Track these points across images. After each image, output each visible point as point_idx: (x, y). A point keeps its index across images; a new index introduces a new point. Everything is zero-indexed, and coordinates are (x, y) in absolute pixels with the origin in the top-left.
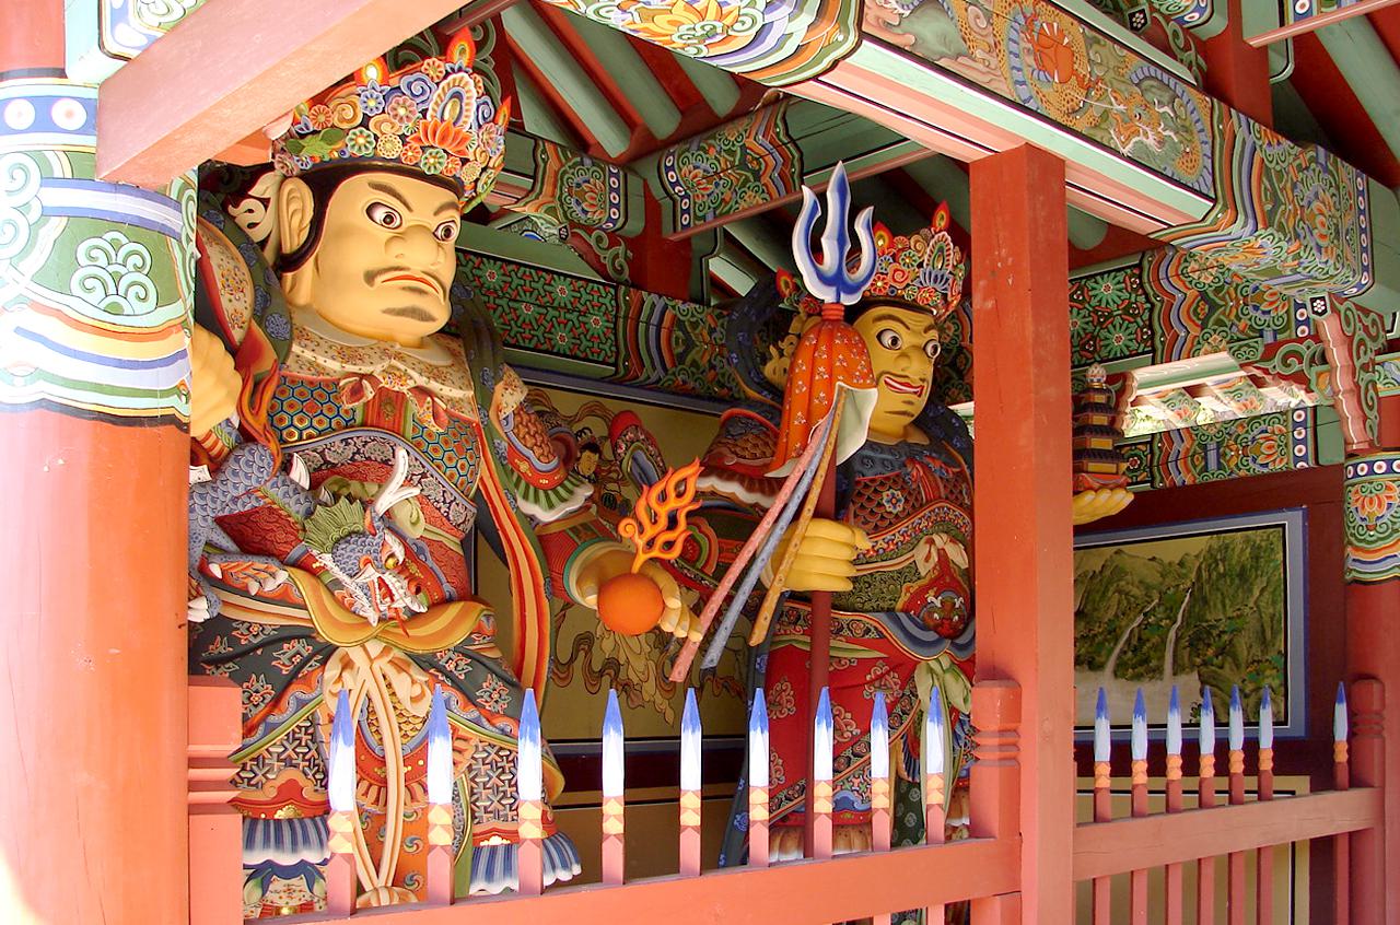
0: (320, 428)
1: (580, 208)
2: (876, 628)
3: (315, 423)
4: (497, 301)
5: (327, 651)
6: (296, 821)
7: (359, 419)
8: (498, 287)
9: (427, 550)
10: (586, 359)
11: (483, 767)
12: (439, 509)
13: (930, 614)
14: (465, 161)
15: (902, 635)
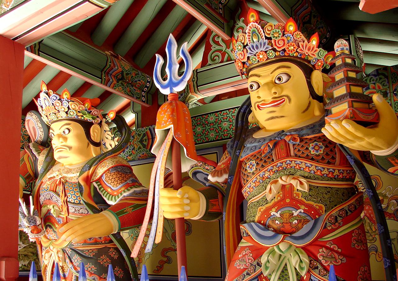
2: (245, 231)
10: (222, 139)
13: (273, 221)
15: (254, 234)
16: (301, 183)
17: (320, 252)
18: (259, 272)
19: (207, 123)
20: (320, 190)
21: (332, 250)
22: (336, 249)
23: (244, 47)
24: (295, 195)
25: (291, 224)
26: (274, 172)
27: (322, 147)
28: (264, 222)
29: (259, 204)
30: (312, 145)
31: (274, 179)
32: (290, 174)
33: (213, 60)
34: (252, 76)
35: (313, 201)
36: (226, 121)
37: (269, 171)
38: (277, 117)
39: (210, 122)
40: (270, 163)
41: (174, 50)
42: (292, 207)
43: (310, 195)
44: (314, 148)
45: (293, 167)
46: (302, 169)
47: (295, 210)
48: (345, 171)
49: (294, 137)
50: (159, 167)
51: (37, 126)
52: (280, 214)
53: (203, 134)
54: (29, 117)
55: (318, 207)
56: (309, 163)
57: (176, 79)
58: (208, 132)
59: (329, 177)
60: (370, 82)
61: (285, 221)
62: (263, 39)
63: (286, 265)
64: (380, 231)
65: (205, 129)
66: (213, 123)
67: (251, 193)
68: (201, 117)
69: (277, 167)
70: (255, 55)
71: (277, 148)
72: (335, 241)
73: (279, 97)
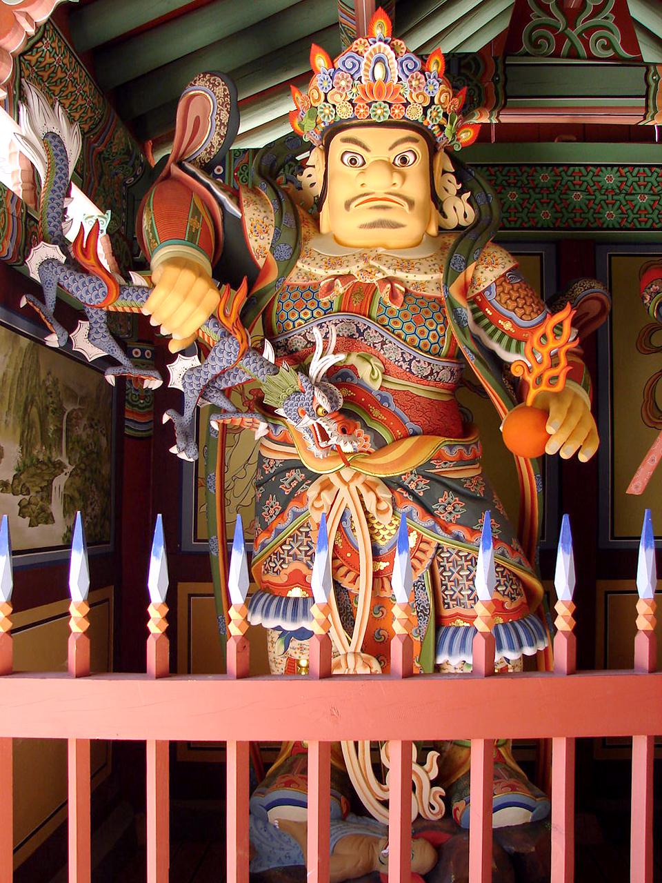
0: (306, 318)
3: (302, 316)
4: (615, 197)
5: (313, 477)
6: (301, 603)
7: (335, 307)
8: (615, 187)
9: (391, 399)
11: (447, 564)
12: (401, 366)
14: (406, 105)
19: (532, 186)
33: (535, 44)
36: (578, 191)
39: (540, 186)
51: (215, 116)
54: (204, 88)
66: (548, 188)
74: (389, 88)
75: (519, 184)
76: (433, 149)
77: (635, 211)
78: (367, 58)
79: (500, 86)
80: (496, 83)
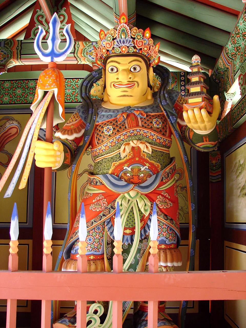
1: (91, 58)
2: (99, 181)
13: (125, 174)
15: (109, 183)
16: (147, 147)
17: (158, 198)
18: (113, 213)
20: (158, 153)
21: (165, 197)
22: (167, 196)
23: (113, 39)
24: (142, 155)
25: (139, 176)
26: (128, 136)
27: (160, 123)
28: (117, 174)
29: (114, 160)
30: (155, 121)
31: (127, 141)
32: (139, 140)
34: (113, 62)
35: (154, 161)
37: (124, 136)
38: (128, 96)
39: (5, 88)
40: (124, 130)
41: (58, 26)
42: (138, 164)
43: (152, 156)
44: (156, 123)
45: (142, 134)
46: (148, 136)
47: (142, 166)
48: (167, 140)
49: (142, 112)
50: (35, 122)
52: (131, 169)
53: (23, 96)
55: (156, 165)
56: (153, 133)
57: (58, 51)
58: (28, 95)
59: (163, 145)
60: (157, 79)
61: (134, 174)
62: (129, 37)
63: (132, 208)
64: (191, 185)
65: (25, 92)
66: (33, 88)
67: (106, 151)
68: (22, 81)
69: (130, 133)
70: (120, 47)
71: (129, 119)
72: (167, 191)
73: (132, 82)
74: (127, 41)
75: (22, 87)
76: (148, 66)
77: (22, 96)
78: (119, 30)
79: (19, 51)
80: (17, 50)
